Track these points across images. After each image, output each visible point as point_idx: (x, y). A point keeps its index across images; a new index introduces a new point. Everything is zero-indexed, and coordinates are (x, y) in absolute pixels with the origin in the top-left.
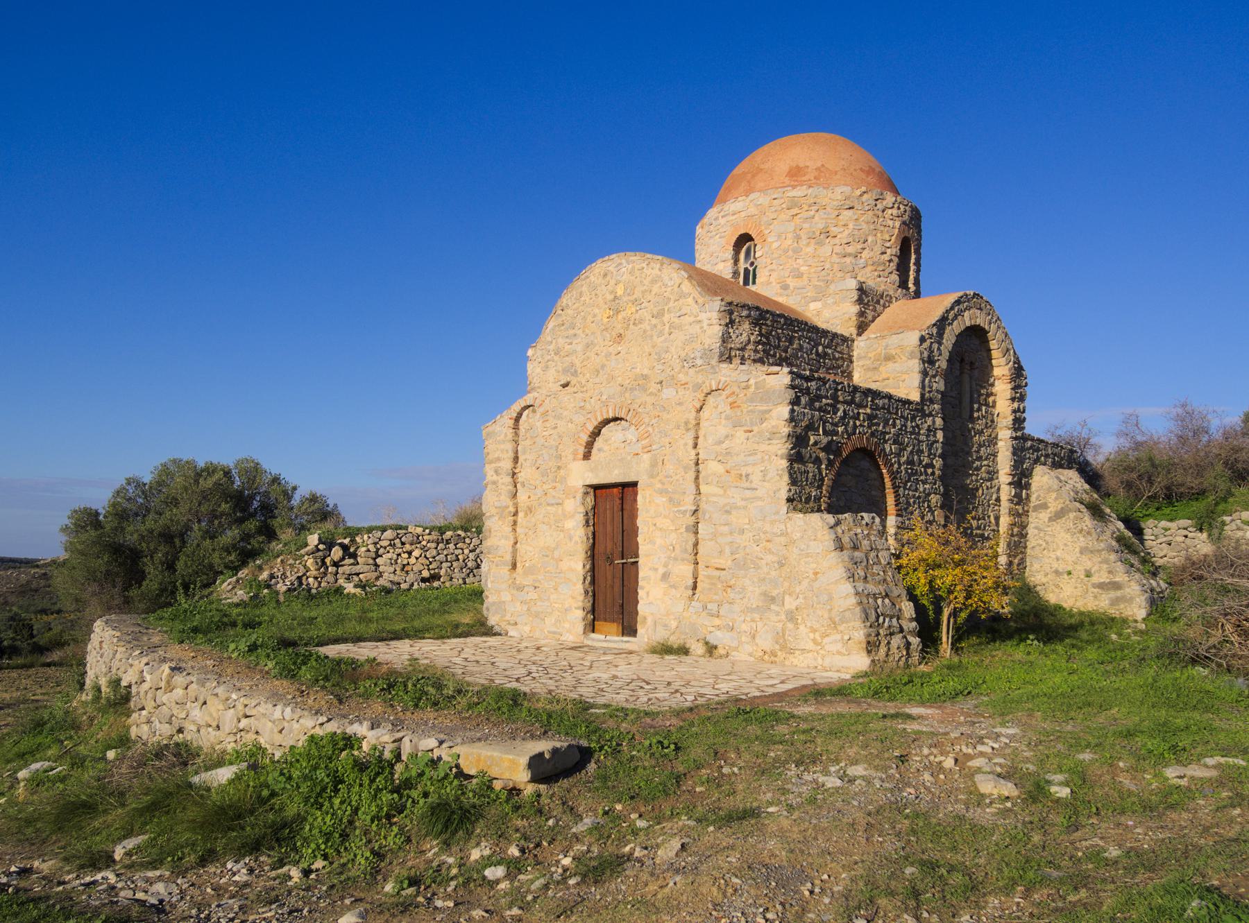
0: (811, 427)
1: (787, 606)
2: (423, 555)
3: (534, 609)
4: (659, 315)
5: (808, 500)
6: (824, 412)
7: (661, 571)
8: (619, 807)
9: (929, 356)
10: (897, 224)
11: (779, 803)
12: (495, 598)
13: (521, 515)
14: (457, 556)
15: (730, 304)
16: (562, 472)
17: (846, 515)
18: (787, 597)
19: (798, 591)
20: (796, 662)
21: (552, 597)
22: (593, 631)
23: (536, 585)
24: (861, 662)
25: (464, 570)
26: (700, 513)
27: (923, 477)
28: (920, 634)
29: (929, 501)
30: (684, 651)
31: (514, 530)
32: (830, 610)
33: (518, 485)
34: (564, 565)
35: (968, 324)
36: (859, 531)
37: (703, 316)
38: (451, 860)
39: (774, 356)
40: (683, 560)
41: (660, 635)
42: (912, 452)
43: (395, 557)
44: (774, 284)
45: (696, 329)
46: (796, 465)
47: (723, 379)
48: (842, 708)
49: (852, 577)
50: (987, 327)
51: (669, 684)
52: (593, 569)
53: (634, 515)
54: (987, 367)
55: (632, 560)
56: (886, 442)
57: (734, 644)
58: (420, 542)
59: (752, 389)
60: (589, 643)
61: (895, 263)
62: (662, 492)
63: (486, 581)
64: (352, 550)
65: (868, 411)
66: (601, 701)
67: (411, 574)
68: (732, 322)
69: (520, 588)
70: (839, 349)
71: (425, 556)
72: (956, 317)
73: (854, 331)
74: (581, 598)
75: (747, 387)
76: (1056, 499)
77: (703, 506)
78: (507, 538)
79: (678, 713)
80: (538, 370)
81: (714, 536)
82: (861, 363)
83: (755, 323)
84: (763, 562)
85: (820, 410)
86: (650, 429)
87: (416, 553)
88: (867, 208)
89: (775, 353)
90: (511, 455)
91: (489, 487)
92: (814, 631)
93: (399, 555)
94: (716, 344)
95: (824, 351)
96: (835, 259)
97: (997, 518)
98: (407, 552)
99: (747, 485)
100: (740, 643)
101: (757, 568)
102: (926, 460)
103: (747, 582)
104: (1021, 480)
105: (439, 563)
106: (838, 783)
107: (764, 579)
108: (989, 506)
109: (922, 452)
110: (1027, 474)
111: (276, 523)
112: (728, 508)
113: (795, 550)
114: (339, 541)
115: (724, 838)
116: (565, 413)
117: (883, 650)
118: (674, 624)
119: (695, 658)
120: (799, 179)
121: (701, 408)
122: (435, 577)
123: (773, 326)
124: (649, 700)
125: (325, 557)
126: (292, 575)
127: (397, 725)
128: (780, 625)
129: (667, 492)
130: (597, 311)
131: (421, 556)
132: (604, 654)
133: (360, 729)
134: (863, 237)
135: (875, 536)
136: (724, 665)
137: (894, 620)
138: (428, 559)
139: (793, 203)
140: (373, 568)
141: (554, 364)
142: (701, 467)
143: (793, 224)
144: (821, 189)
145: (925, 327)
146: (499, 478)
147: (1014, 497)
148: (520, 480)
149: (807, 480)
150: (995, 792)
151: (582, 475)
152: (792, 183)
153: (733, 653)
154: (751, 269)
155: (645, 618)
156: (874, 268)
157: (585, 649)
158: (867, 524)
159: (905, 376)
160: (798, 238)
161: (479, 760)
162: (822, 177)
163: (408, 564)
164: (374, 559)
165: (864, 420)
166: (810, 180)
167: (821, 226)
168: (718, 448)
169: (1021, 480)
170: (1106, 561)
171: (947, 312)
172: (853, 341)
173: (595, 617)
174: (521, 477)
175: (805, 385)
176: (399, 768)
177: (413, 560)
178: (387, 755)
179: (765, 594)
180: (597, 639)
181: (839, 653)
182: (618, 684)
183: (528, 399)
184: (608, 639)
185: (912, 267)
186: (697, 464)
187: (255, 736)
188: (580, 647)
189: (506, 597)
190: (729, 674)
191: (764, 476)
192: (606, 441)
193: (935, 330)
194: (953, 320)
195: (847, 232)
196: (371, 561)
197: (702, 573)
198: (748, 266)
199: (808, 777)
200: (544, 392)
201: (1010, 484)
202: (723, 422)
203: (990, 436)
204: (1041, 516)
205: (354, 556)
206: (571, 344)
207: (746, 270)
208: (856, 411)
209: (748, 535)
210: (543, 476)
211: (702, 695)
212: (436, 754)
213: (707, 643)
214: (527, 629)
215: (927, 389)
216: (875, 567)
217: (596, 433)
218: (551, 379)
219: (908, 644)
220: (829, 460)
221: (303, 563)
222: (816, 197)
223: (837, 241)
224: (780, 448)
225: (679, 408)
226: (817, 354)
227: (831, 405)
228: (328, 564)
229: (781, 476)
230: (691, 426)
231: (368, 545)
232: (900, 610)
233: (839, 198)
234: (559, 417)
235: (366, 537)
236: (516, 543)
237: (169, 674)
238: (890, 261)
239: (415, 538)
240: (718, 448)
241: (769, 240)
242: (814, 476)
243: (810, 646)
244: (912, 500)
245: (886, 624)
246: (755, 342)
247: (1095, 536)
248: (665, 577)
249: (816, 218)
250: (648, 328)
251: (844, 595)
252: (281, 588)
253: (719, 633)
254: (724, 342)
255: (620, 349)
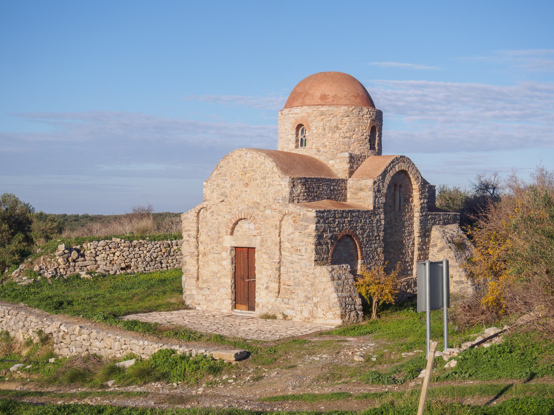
0: (325, 231)
1: (314, 301)
2: (121, 255)
3: (208, 298)
4: (264, 178)
5: (323, 259)
6: (330, 223)
7: (265, 285)
8: (259, 367)
9: (378, 189)
10: (369, 121)
11: (302, 364)
12: (189, 292)
13: (200, 256)
14: (140, 255)
15: (293, 179)
16: (221, 240)
17: (336, 266)
18: (314, 297)
19: (318, 295)
20: (317, 322)
21: (216, 293)
22: (235, 308)
23: (209, 288)
24: (339, 322)
25: (144, 263)
26: (281, 263)
27: (374, 242)
28: (363, 310)
29: (377, 251)
30: (274, 317)
31: (198, 263)
32: (329, 303)
33: (199, 243)
34: (222, 280)
35: (397, 170)
36: (341, 272)
37: (282, 183)
38: (218, 379)
39: (312, 196)
40: (274, 281)
41: (265, 311)
42: (369, 232)
43: (106, 256)
44: (314, 149)
45: (279, 188)
46: (318, 247)
47: (290, 210)
48: (327, 338)
49: (337, 291)
50: (407, 170)
51: (270, 331)
52: (235, 282)
53: (254, 261)
54: (410, 185)
55: (253, 280)
56: (357, 230)
57: (294, 315)
58: (119, 247)
59: (302, 216)
60: (234, 313)
61: (368, 139)
62: (265, 253)
63: (185, 284)
64: (82, 252)
65: (349, 219)
66: (249, 338)
67: (115, 266)
68: (294, 186)
69: (201, 289)
70: (340, 186)
71: (123, 255)
72: (391, 169)
73: (347, 175)
74: (230, 295)
75: (300, 215)
76: (440, 242)
77: (283, 260)
78: (194, 266)
79: (274, 341)
80: (208, 192)
81: (287, 272)
82: (350, 190)
83: (304, 184)
84: (306, 284)
85: (328, 223)
86: (260, 226)
87: (117, 254)
88: (355, 116)
89: (312, 195)
90: (196, 229)
91: (185, 242)
92: (323, 310)
93: (108, 255)
94: (288, 196)
95: (333, 188)
96: (341, 139)
97: (413, 253)
98: (112, 253)
99: (300, 254)
100: (297, 314)
101: (303, 286)
102: (376, 234)
103: (299, 291)
104: (425, 233)
105: (130, 259)
106: (319, 359)
107: (306, 291)
108: (409, 247)
109: (374, 231)
110: (430, 230)
111: (32, 234)
112: (292, 262)
113: (317, 280)
114: (74, 247)
115: (288, 371)
116: (222, 213)
117: (347, 317)
118: (270, 307)
119: (279, 320)
120: (325, 101)
121: (282, 220)
122: (128, 267)
123: (311, 184)
124: (264, 337)
125: (68, 257)
126: (51, 268)
127: (187, 346)
128: (311, 308)
129: (268, 253)
130: (236, 171)
131: (120, 255)
132: (242, 319)
133: (176, 347)
134: (353, 129)
135: (348, 273)
136: (290, 323)
137: (353, 306)
138: (124, 257)
139: (322, 114)
140: (94, 262)
141: (216, 190)
142: (282, 244)
143: (322, 123)
144: (334, 108)
145: (376, 176)
146: (190, 239)
147: (421, 242)
148: (200, 240)
149: (323, 252)
150: (358, 360)
151: (229, 242)
152: (322, 103)
153: (294, 318)
154: (304, 139)
155: (258, 304)
156: (358, 142)
157: (233, 316)
158: (345, 269)
159: (368, 198)
160: (324, 129)
161: (219, 355)
162: (335, 103)
163: (113, 260)
164: (95, 257)
165: (347, 223)
166: (330, 102)
167: (334, 124)
168: (289, 237)
169: (425, 233)
170: (458, 271)
171: (387, 168)
172: (347, 180)
173: (236, 303)
174: (201, 239)
175: (322, 215)
176: (191, 358)
177: (116, 258)
178: (188, 354)
179: (306, 296)
180: (237, 312)
181: (332, 319)
182: (252, 332)
183: (204, 204)
184: (242, 312)
185: (377, 138)
186: (280, 243)
187: (131, 351)
188: (231, 316)
189: (194, 292)
190: (291, 327)
191: (306, 251)
192: (241, 227)
193: (381, 177)
194: (390, 171)
195: (346, 127)
196: (93, 259)
197: (282, 287)
198: (302, 137)
199: (311, 358)
200: (212, 202)
201: (419, 237)
202: (291, 227)
203: (410, 216)
204: (434, 249)
205: (83, 256)
206: (224, 183)
207: (302, 139)
208: (343, 220)
209: (300, 273)
210: (211, 240)
211: (282, 336)
212: (205, 354)
213: (284, 314)
214: (205, 306)
215: (377, 204)
216: (346, 286)
217: (236, 223)
218: (215, 197)
219: (358, 315)
220: (332, 243)
221: (56, 260)
222: (332, 111)
223: (341, 131)
224: (312, 240)
225: (273, 219)
226: (331, 190)
227: (333, 220)
228: (70, 261)
229: (312, 251)
230: (278, 227)
231: (90, 249)
232: (355, 302)
233: (343, 112)
234: (219, 215)
235: (89, 244)
236: (198, 269)
237: (80, 329)
238: (366, 138)
239: (117, 245)
240: (289, 237)
241: (312, 129)
242: (326, 250)
243: (322, 316)
244: (368, 252)
245: (349, 308)
246: (303, 192)
247: (455, 260)
248: (267, 288)
249: (332, 120)
250: (259, 183)
251: (334, 297)
252: (48, 275)
253: (288, 311)
254: (291, 194)
255: (247, 189)
